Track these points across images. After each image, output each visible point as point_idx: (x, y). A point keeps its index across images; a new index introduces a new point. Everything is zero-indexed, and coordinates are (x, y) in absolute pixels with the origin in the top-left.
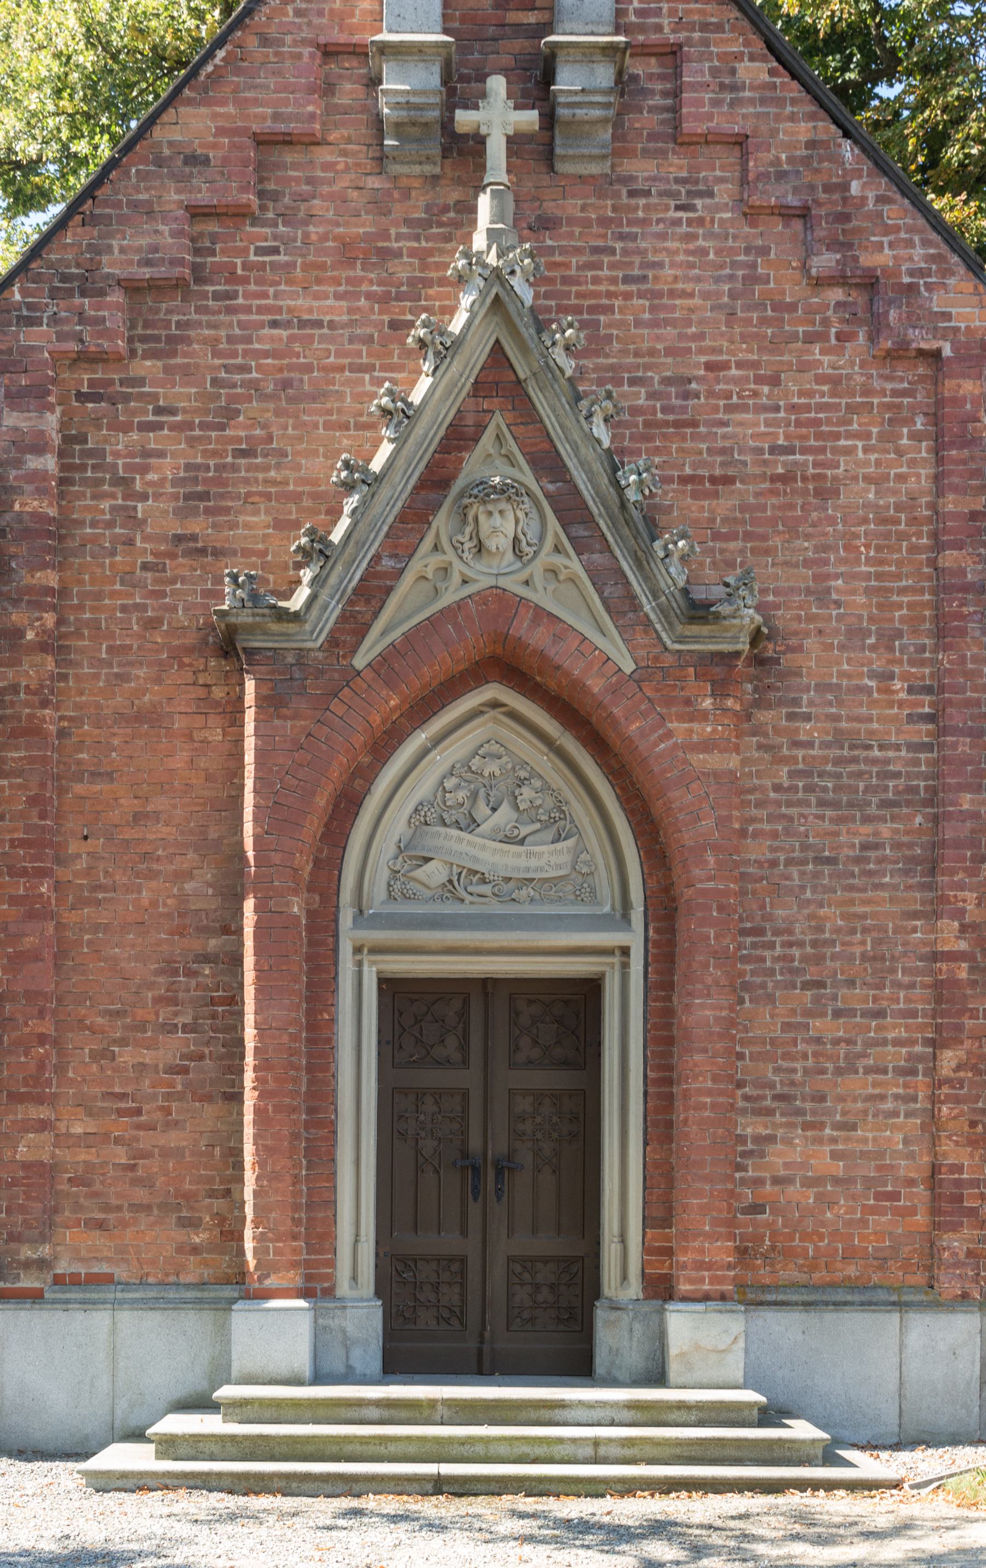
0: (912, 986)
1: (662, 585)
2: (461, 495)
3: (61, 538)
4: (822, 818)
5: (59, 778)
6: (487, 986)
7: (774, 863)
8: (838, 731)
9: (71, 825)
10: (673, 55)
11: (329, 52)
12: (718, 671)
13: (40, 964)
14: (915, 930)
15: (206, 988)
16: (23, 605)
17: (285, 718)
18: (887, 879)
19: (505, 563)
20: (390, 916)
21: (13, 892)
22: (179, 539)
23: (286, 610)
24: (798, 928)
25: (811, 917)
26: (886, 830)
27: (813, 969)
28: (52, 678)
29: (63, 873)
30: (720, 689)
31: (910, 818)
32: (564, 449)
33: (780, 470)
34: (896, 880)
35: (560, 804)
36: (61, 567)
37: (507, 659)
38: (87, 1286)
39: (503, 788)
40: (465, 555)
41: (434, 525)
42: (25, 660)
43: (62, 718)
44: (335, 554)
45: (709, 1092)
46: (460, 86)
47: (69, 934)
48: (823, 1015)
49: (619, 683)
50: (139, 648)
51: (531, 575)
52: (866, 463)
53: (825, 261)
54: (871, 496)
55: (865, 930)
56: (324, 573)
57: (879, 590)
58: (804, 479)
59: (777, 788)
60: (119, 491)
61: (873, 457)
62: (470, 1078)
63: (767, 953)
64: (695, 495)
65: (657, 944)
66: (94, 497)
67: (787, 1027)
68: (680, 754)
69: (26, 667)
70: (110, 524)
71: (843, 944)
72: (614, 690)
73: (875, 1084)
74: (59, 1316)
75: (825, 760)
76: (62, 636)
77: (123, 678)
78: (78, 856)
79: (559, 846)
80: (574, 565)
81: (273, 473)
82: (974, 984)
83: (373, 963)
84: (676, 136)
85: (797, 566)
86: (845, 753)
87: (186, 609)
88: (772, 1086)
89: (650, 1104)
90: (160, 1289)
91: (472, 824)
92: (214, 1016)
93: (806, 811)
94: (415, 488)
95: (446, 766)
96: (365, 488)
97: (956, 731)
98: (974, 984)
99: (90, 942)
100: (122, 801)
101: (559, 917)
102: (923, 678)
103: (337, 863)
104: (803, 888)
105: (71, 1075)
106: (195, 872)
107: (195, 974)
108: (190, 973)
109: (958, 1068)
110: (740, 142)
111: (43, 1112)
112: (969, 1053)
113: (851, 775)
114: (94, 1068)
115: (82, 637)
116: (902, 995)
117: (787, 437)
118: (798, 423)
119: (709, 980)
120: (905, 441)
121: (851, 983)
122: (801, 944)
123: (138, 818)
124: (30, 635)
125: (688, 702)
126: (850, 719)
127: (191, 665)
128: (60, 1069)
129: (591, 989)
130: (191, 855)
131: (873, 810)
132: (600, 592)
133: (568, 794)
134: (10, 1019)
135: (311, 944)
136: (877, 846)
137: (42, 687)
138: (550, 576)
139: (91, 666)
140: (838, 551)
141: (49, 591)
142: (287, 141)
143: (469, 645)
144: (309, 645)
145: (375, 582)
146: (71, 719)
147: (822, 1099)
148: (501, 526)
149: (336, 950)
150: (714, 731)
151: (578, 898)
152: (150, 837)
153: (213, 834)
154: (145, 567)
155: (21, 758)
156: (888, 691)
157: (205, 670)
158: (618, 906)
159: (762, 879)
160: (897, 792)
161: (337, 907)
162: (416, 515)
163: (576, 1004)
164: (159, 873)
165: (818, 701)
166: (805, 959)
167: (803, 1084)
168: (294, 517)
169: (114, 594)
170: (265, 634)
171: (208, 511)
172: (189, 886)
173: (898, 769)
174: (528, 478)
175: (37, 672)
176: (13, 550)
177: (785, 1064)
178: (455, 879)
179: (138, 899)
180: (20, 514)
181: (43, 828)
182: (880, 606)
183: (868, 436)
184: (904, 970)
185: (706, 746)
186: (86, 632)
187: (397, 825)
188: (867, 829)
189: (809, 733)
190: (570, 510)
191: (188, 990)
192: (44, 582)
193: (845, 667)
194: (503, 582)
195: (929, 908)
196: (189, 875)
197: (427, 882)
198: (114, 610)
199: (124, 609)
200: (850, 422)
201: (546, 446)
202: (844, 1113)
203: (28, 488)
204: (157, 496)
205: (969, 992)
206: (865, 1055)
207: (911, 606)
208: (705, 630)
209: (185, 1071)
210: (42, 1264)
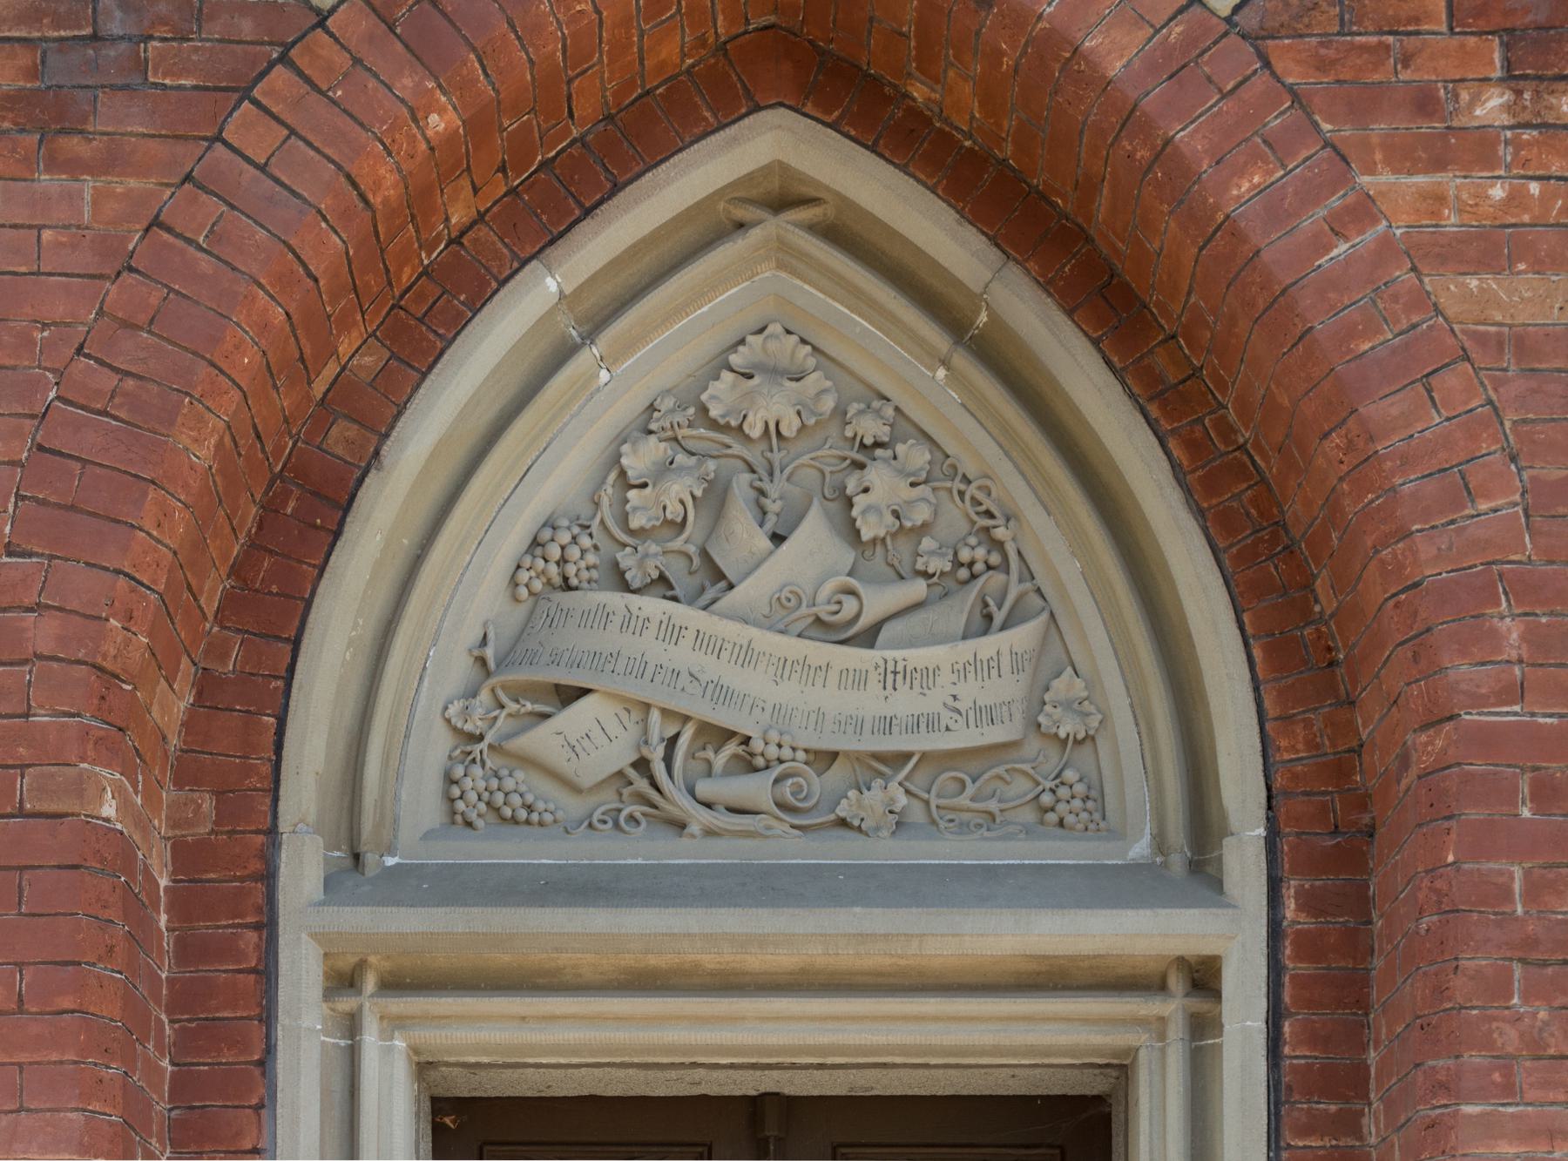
17: (74, 167)
39: (809, 476)
65: (1309, 947)
68: (1402, 274)
72: (1177, 67)
79: (987, 646)
83: (395, 1023)
95: (627, 407)
101: (990, 872)
119: (1509, 1038)
133: (1014, 488)
135: (186, 951)
149: (266, 973)
150: (1516, 199)
151: (1047, 815)
158: (1177, 834)
161: (273, 832)
178: (657, 755)
187: (472, 591)
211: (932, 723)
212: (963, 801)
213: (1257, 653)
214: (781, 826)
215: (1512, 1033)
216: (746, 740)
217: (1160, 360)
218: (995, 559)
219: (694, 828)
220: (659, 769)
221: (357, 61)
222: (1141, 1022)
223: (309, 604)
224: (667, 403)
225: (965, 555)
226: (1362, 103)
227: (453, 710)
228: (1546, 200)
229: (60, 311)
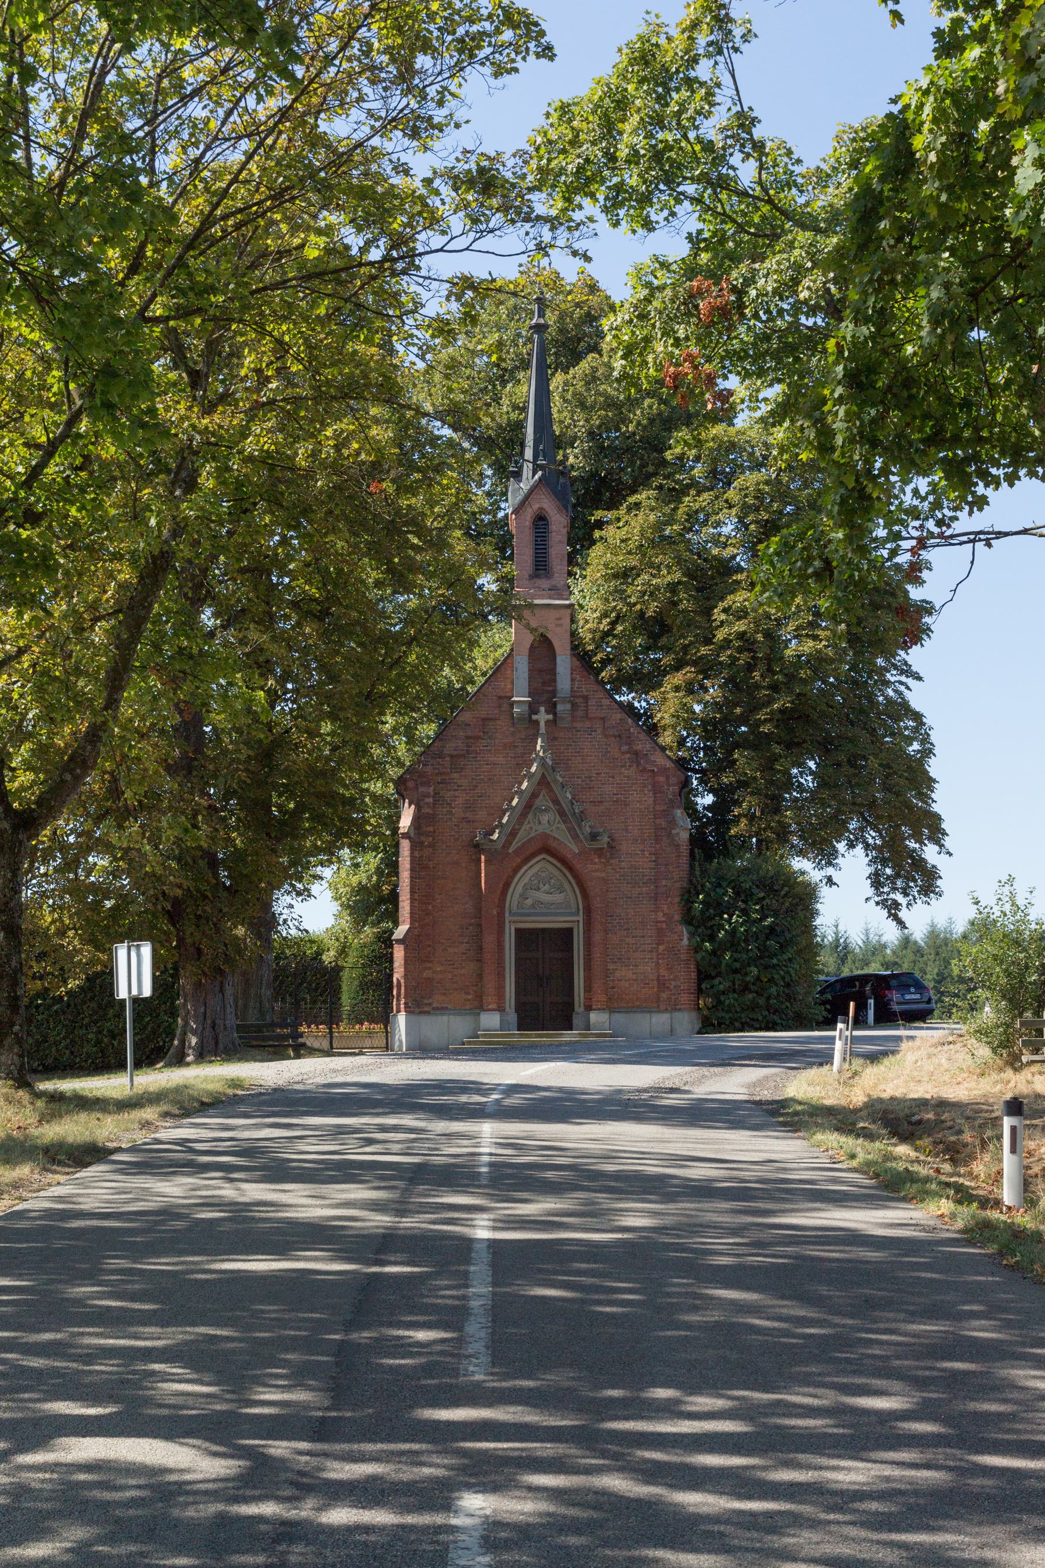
6: (543, 930)
10: (586, 698)
11: (500, 698)
37: (546, 848)
38: (441, 1010)
46: (533, 709)
53: (625, 748)
74: (434, 1018)
80: (563, 826)
84: (587, 717)
90: (459, 1010)
91: (538, 889)
103: (504, 900)
110: (603, 719)
111: (429, 965)
129: (570, 931)
142: (490, 719)
148: (545, 818)
162: (524, 815)
163: (566, 935)
185: (596, 871)
187: (520, 889)
190: (562, 813)
210: (430, 1004)
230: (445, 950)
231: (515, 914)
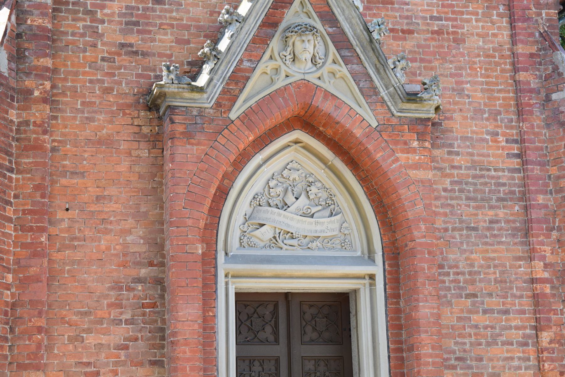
0: (521, 297)
1: (393, 82)
2: (285, 31)
3: (54, 41)
4: (469, 206)
5: (51, 175)
7: (446, 230)
8: (473, 161)
9: (58, 202)
12: (420, 128)
13: (40, 284)
14: (520, 267)
15: (139, 298)
16: (33, 76)
17: (192, 144)
18: (504, 239)
19: (308, 67)
20: (243, 256)
21: (24, 241)
22: (122, 45)
23: (197, 87)
24: (461, 264)
25: (467, 259)
26: (501, 213)
27: (470, 287)
28: (48, 118)
29: (53, 230)
30: (421, 137)
31: (512, 207)
32: (337, 11)
33: (436, 29)
34: (509, 240)
35: (331, 196)
36: (54, 56)
37: (310, 120)
40: (287, 62)
41: (271, 46)
42: (33, 107)
43: (53, 141)
44: (222, 58)
45: (431, 356)
47: (56, 266)
48: (477, 312)
49: (370, 132)
50: (100, 103)
51: (322, 74)
52: (477, 27)
54: (481, 43)
55: (495, 266)
56: (217, 67)
57: (488, 90)
58: (448, 33)
59: (445, 190)
60: (88, 18)
61: (480, 24)
62: (280, 350)
63: (446, 278)
64: (394, 38)
65: (390, 273)
66: (73, 20)
67: (459, 319)
68: (403, 170)
69: (34, 111)
70: (83, 35)
71: (485, 274)
72: (368, 135)
73: (508, 351)
75: (468, 176)
76: (53, 95)
77: (90, 119)
78: (63, 220)
79: (333, 218)
80: (344, 70)
81: (174, 14)
82: (554, 295)
83: (233, 283)
85: (447, 77)
86: (478, 172)
87: (127, 84)
88: (454, 352)
89: (391, 364)
91: (285, 206)
92: (144, 314)
93: (460, 202)
94: (260, 26)
96: (238, 24)
97: (533, 163)
98: (554, 295)
99: (69, 271)
100: (89, 189)
102: (513, 135)
104: (462, 243)
105: (56, 352)
106: (132, 230)
107: (133, 289)
108: (129, 289)
109: (551, 342)
112: (555, 333)
113: (481, 184)
114: (71, 347)
115: (66, 95)
116: (517, 301)
117: (438, 12)
118: (443, 6)
119: (426, 292)
120: (495, 17)
121: (490, 295)
122: (463, 274)
123: (98, 198)
124: (36, 93)
125: (405, 143)
126: (479, 155)
127: (130, 114)
128: (50, 348)
130: (130, 220)
131: (493, 203)
132: (358, 85)
133: (335, 190)
134: (20, 318)
136: (497, 222)
137: (44, 122)
138: (331, 75)
139: (71, 112)
140: (466, 70)
141: (47, 69)
143: (291, 108)
144: (207, 105)
145: (240, 74)
146: (59, 142)
147: (481, 360)
148: (307, 47)
149: (216, 275)
150: (420, 159)
152: (106, 210)
153: (143, 209)
154: (103, 59)
155: (30, 163)
156: (496, 141)
157: (138, 117)
159: (441, 238)
160: (505, 194)
161: (216, 251)
162: (261, 40)
163: (337, 309)
164: (111, 230)
165: (462, 145)
166: (466, 282)
167: (470, 351)
168: (186, 38)
169: (84, 73)
170: (182, 98)
171: (138, 32)
172: (129, 239)
173: (504, 181)
174: (319, 25)
175: (41, 114)
176: (26, 45)
177: (460, 340)
178: (277, 236)
179: (99, 246)
180: (31, 26)
181: (43, 204)
182: (489, 98)
183: (477, 14)
184: (517, 288)
186: (68, 93)
187: (244, 207)
188: (492, 212)
189: (459, 161)
190: (341, 42)
191: (128, 299)
192: (45, 64)
193: (474, 128)
194: (307, 77)
195: (526, 255)
196: (129, 232)
197: (261, 238)
198: (85, 82)
199: (91, 81)
200: (468, 7)
201: (327, 9)
202: (493, 368)
203: (36, 12)
204: (110, 22)
205: (552, 300)
206: (501, 335)
207: (504, 99)
208: (413, 106)
209: (126, 348)
211: (324, 231)
212: (329, 244)
213: (379, 223)
214: (299, 248)
215: (427, 292)
216: (292, 233)
217: (361, 174)
218: (332, 203)
219: (284, 249)
220: (278, 238)
221: (238, 129)
222: (361, 284)
223: (221, 211)
224: (276, 174)
225: (328, 202)
226: (396, 143)
227: (241, 227)
228: (424, 159)
229: (191, 168)
230: (77, 339)
231: (236, 259)
